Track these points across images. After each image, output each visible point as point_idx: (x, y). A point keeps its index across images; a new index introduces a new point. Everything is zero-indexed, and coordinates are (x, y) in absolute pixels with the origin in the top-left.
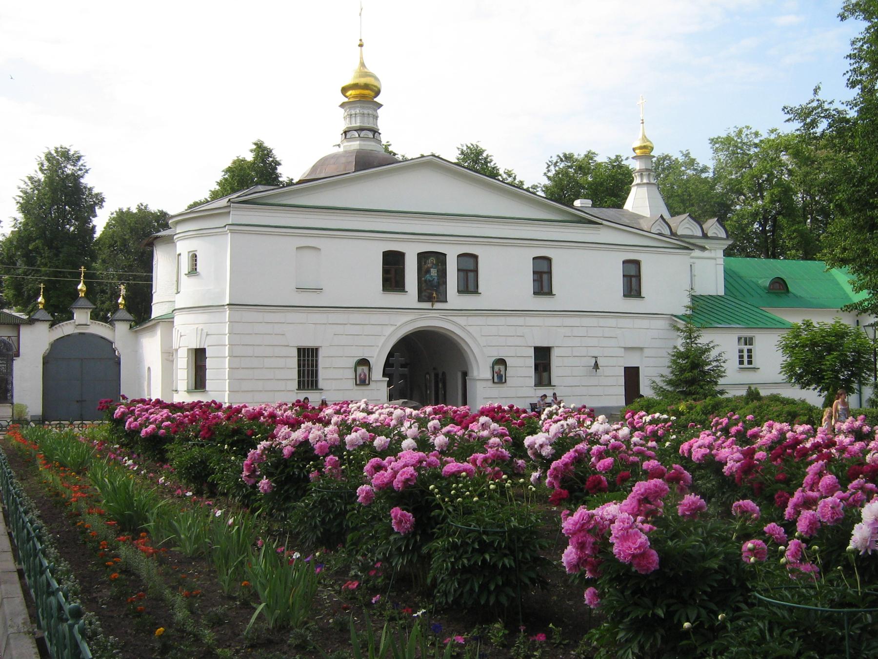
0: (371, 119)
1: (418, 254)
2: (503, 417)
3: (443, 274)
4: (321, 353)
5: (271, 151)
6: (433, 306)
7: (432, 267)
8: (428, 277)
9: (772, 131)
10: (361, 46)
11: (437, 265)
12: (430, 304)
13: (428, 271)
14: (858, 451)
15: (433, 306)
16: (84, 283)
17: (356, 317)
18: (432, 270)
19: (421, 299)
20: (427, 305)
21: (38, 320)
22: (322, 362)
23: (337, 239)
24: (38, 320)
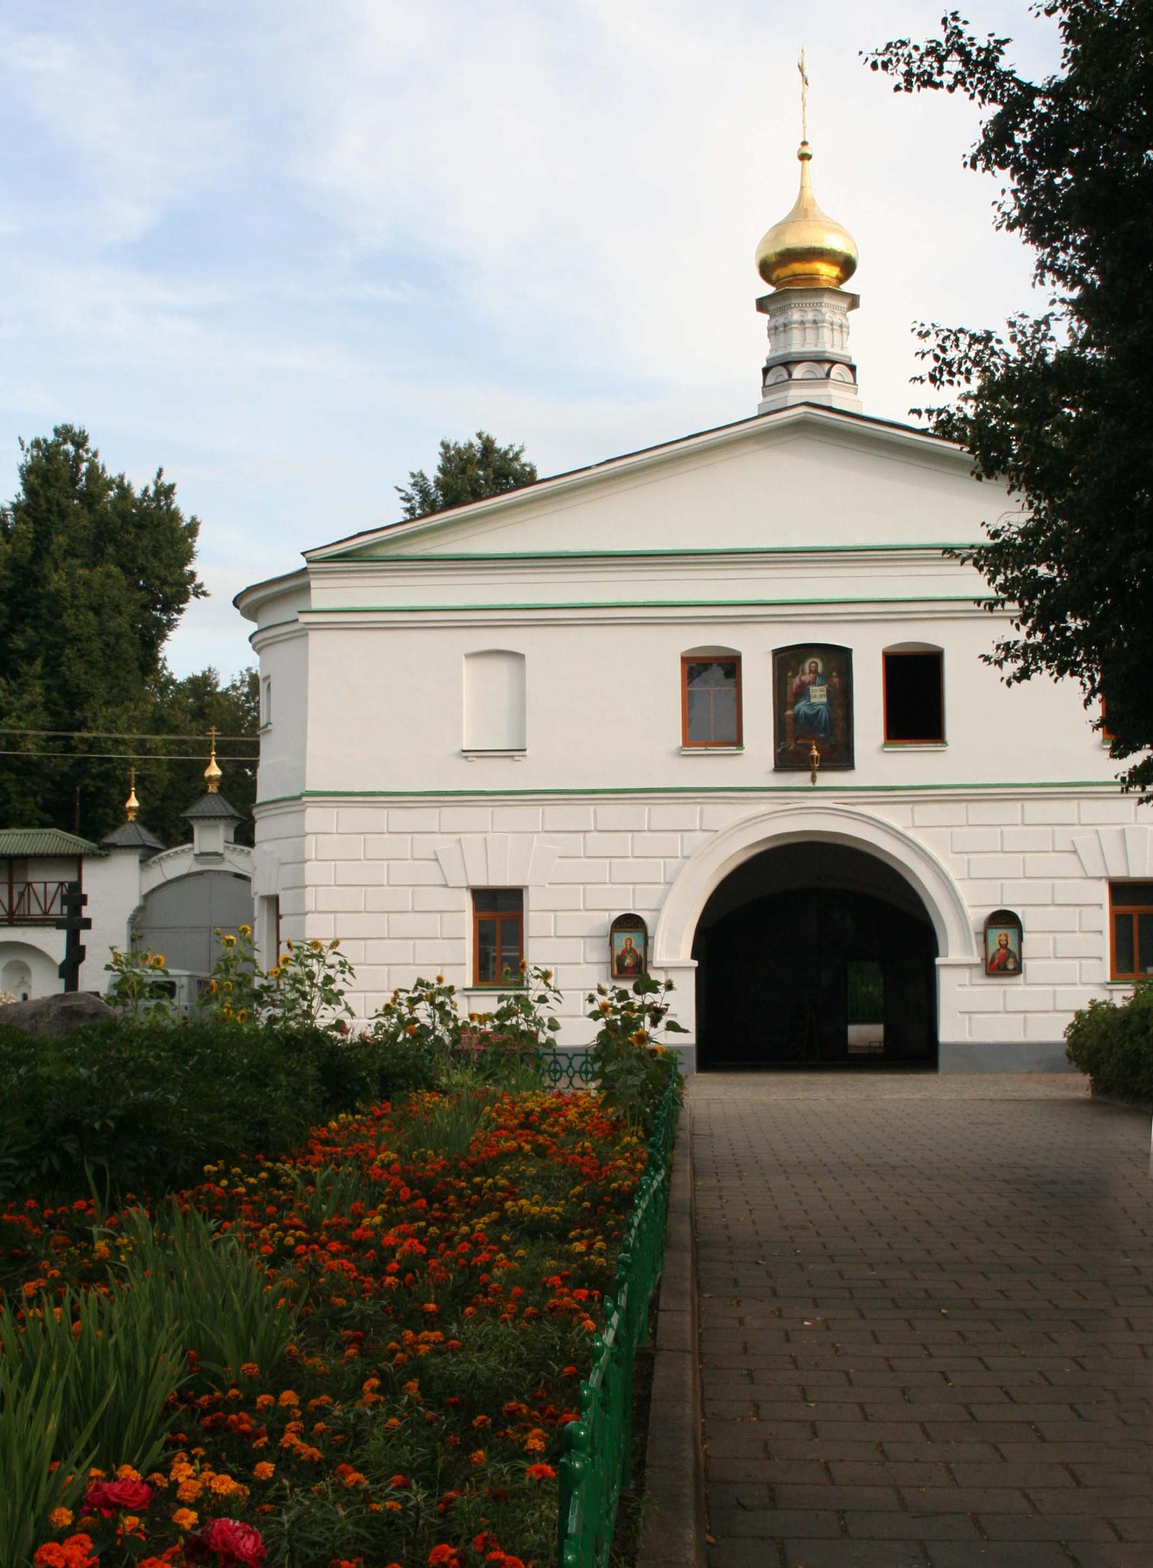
0: (837, 334)
1: (777, 653)
2: (220, 1111)
3: (843, 697)
4: (532, 902)
5: (488, 446)
6: (813, 779)
7: (814, 683)
8: (802, 707)
9: (981, 122)
10: (804, 157)
11: (825, 678)
12: (808, 775)
13: (802, 692)
14: (293, 1390)
15: (813, 779)
16: (219, 763)
17: (611, 813)
18: (812, 688)
19: (785, 761)
20: (800, 779)
21: (114, 846)
22: (534, 922)
23: (280, 646)
24: (114, 846)
